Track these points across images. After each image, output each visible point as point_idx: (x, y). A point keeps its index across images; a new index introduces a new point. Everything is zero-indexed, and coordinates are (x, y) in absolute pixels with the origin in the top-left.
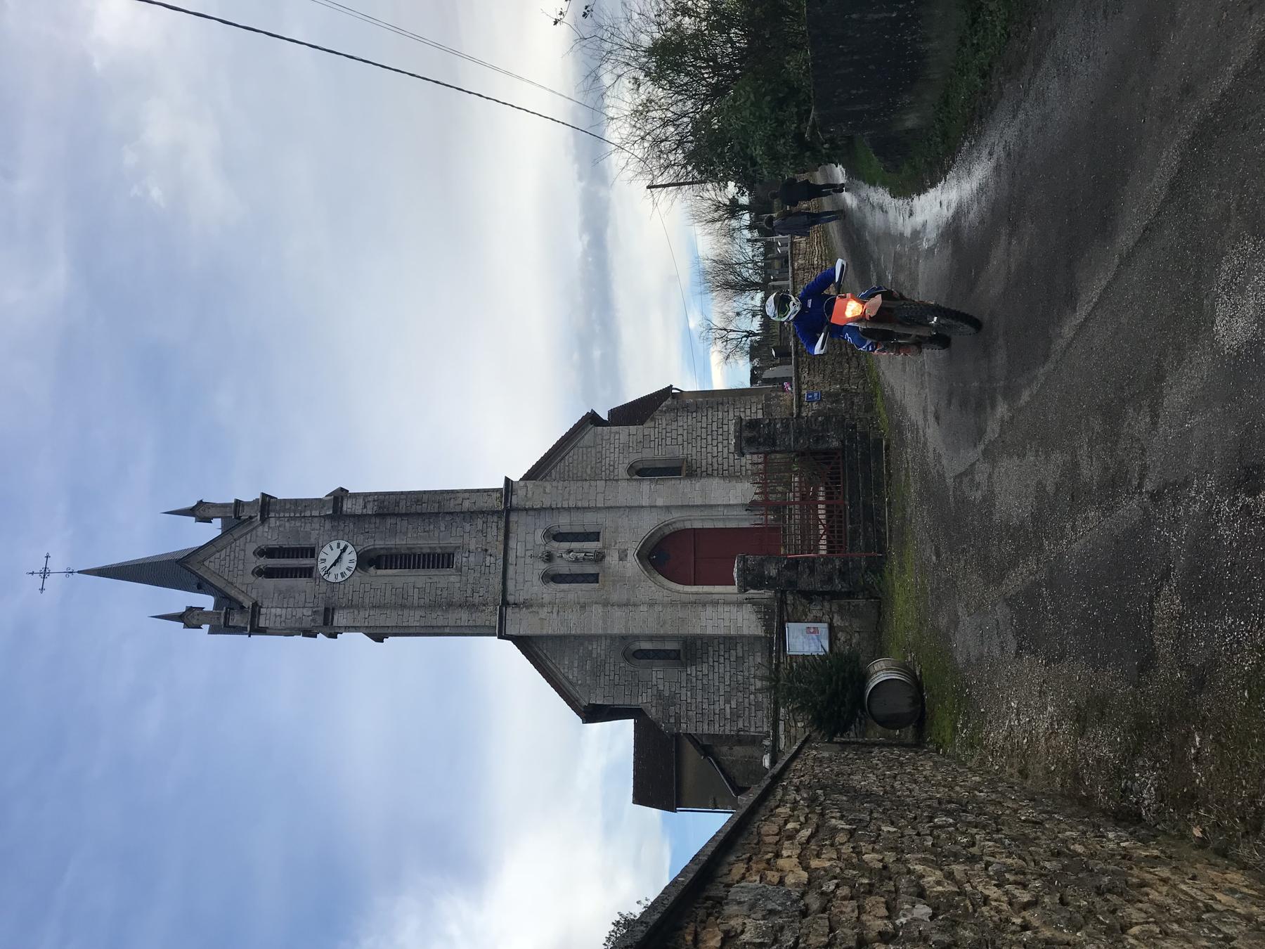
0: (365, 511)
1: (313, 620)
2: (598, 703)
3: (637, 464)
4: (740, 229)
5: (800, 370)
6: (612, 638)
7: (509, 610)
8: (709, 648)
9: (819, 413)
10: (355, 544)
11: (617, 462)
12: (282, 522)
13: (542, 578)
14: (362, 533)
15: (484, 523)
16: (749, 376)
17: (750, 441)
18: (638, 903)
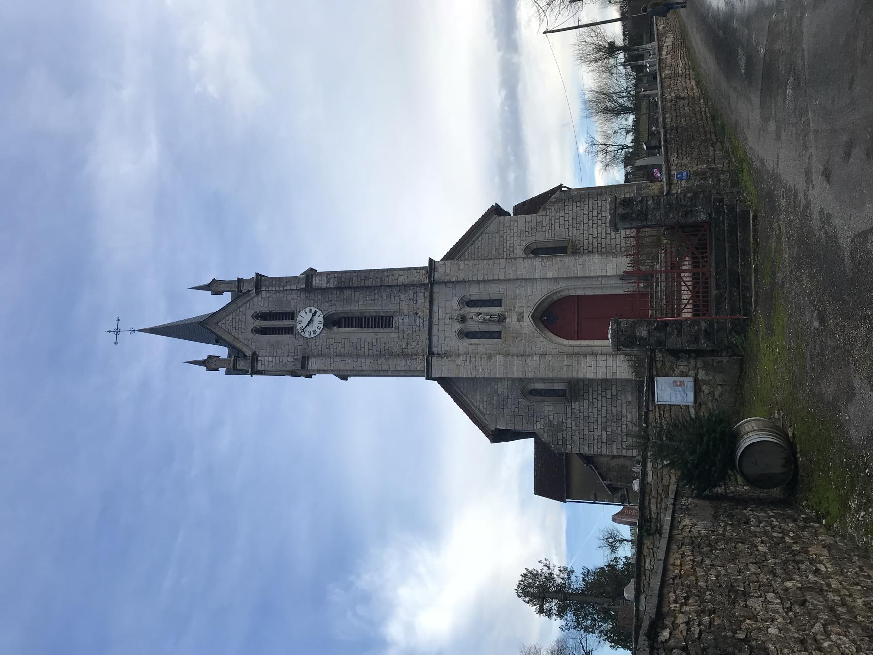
0: (328, 285)
1: (294, 365)
2: (502, 428)
3: (532, 245)
4: (616, 66)
5: (669, 154)
6: (513, 380)
7: (434, 358)
9: (688, 190)
11: (516, 244)
12: (270, 294)
13: (458, 335)
14: (327, 302)
15: (414, 293)
17: (624, 218)
18: (539, 562)
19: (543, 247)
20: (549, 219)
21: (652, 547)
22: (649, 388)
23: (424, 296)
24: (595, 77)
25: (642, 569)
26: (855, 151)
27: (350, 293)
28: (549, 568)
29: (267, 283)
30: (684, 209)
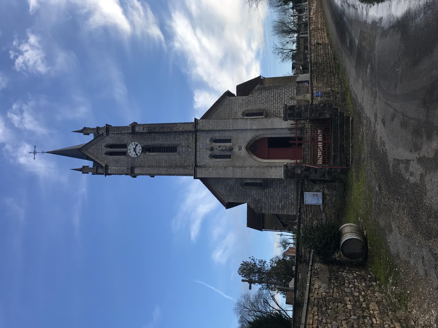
2: (231, 202)
3: (245, 112)
4: (288, 9)
5: (313, 80)
6: (237, 178)
7: (198, 169)
8: (274, 182)
9: (321, 102)
10: (140, 143)
11: (238, 111)
12: (114, 135)
14: (143, 139)
16: (292, 66)
18: (249, 258)
19: (252, 112)
20: (254, 99)
21: (302, 269)
22: (301, 197)
23: (192, 137)
24: (278, 15)
25: (297, 278)
26: (396, 119)
27: (155, 135)
28: (254, 260)
29: (112, 129)
30: (319, 112)
